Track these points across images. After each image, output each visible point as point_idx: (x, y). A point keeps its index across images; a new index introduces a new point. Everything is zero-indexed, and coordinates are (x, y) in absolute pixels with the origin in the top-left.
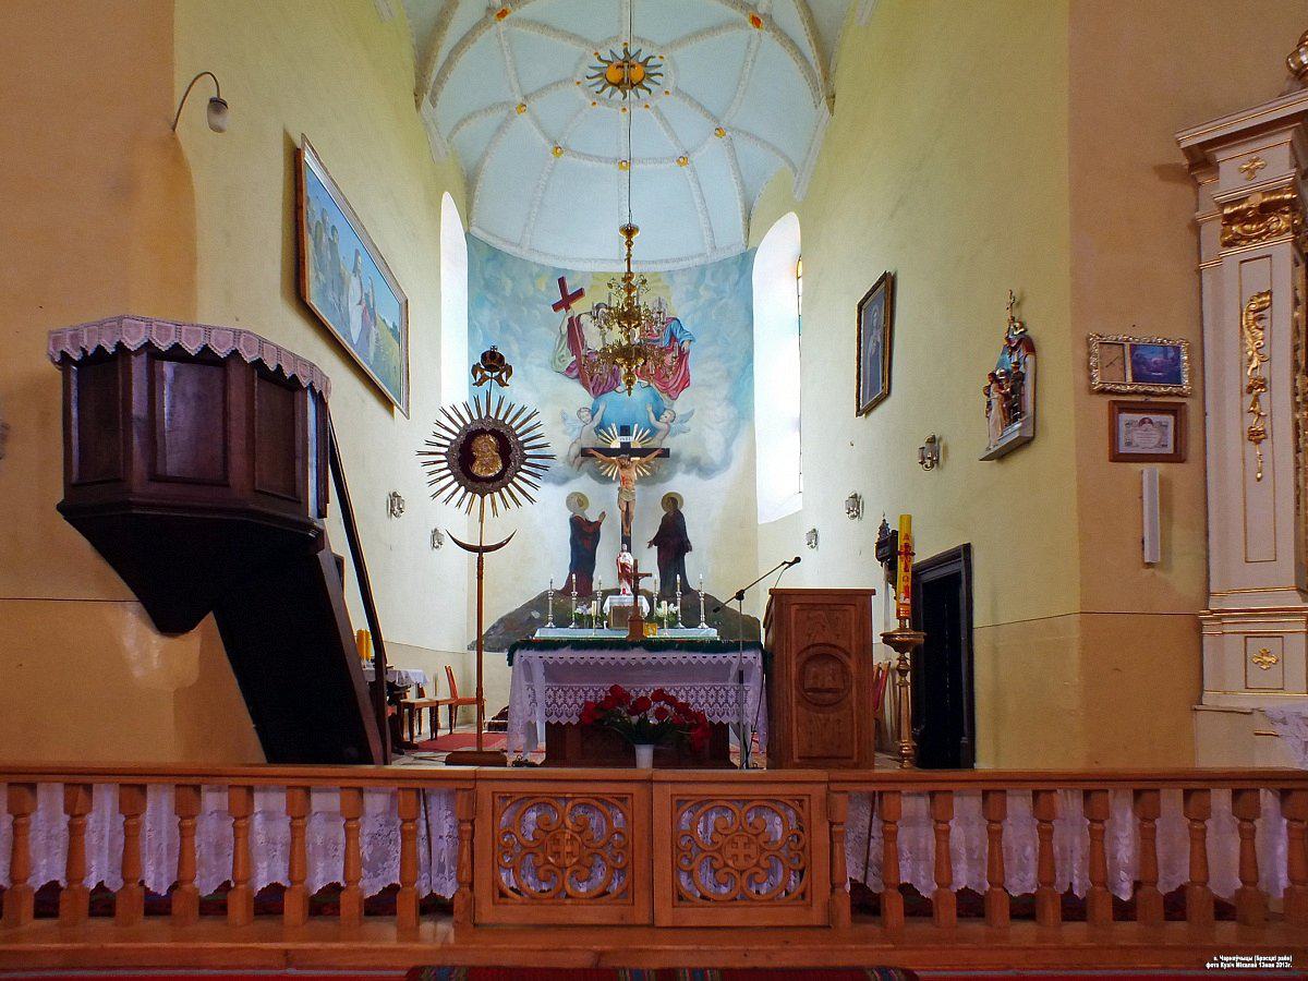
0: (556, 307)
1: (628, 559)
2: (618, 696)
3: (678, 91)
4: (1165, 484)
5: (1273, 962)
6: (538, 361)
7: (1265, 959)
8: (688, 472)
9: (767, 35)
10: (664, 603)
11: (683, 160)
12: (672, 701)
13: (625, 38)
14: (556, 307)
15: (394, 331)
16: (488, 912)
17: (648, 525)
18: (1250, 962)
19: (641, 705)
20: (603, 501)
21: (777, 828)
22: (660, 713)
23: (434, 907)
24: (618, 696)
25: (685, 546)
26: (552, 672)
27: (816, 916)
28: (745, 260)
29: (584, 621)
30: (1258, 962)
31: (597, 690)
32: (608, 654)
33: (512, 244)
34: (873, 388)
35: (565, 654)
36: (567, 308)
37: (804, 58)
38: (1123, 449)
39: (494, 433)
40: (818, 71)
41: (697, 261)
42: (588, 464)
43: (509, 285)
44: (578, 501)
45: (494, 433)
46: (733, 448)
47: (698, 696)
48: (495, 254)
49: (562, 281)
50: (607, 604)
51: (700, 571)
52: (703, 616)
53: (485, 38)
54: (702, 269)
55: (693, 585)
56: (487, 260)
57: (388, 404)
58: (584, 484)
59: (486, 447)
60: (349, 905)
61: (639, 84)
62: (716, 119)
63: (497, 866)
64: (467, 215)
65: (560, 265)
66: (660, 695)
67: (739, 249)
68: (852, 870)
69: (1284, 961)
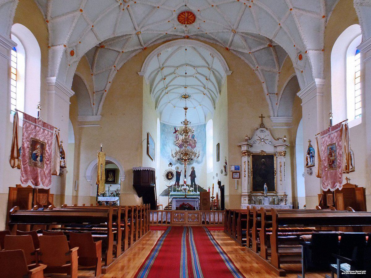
0: (174, 133)
1: (185, 180)
2: (183, 204)
3: (193, 99)
4: (238, 181)
5: (361, 272)
6: (171, 143)
7: (358, 271)
8: (196, 163)
9: (206, 96)
10: (191, 188)
11: (195, 108)
12: (189, 204)
13: (185, 93)
14: (174, 133)
15: (154, 149)
16: (173, 222)
17: (189, 173)
18: (354, 272)
19: (186, 205)
20: (181, 168)
21: (196, 215)
22: (188, 206)
23: (168, 223)
24: (183, 204)
25: (195, 177)
26: (177, 201)
27: (199, 223)
28: (205, 125)
29: (178, 191)
30: (356, 272)
31: (182, 203)
32: (183, 199)
33: (167, 123)
34: (218, 159)
35: (178, 199)
36: (176, 133)
37: (214, 86)
38: (234, 177)
39: (171, 173)
40: (218, 91)
41: (197, 124)
42: (179, 161)
43: (166, 130)
44: (178, 168)
45: (171, 173)
46: (203, 159)
47: (192, 204)
48: (164, 125)
49: (175, 128)
50: (182, 188)
51: (198, 181)
52: (197, 190)
53: (165, 96)
54: (198, 126)
55: (197, 183)
56: (163, 126)
57: (152, 160)
58: (178, 165)
59: (170, 174)
60: (162, 222)
61: (187, 97)
62: (200, 103)
63: (174, 219)
64: (160, 120)
65: (175, 125)
66: (188, 204)
67: (203, 123)
68: (203, 220)
69: (364, 272)
